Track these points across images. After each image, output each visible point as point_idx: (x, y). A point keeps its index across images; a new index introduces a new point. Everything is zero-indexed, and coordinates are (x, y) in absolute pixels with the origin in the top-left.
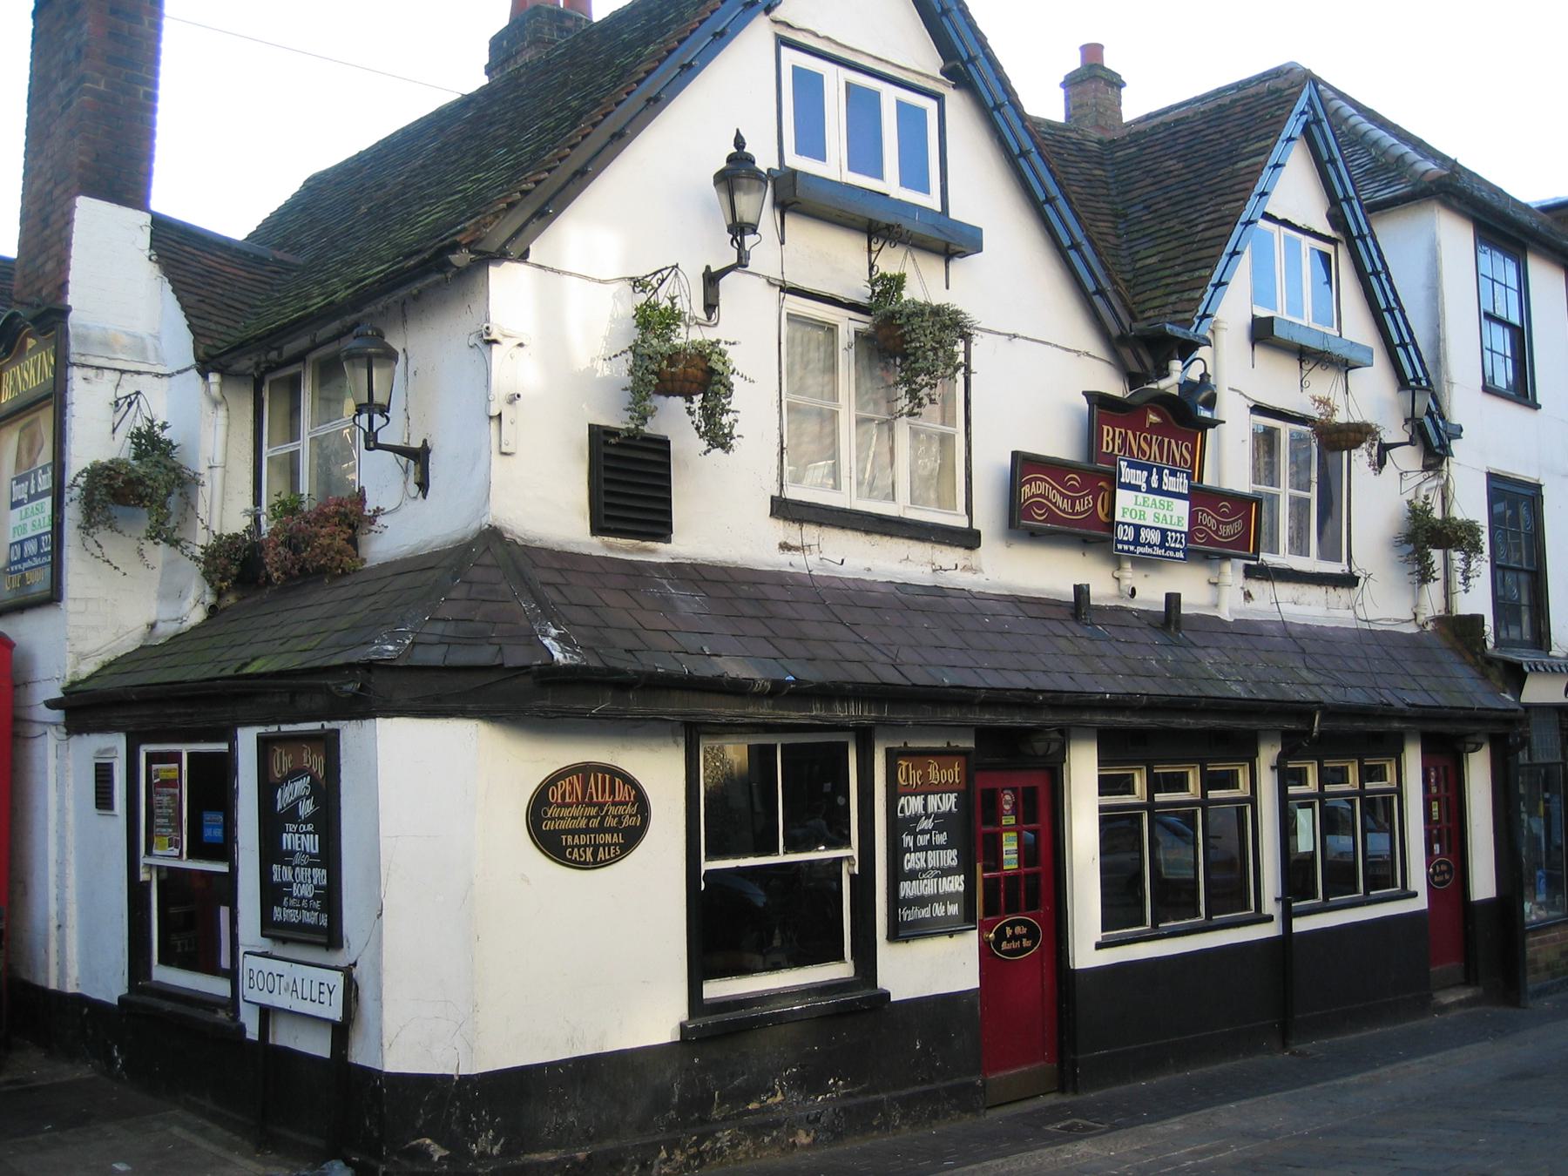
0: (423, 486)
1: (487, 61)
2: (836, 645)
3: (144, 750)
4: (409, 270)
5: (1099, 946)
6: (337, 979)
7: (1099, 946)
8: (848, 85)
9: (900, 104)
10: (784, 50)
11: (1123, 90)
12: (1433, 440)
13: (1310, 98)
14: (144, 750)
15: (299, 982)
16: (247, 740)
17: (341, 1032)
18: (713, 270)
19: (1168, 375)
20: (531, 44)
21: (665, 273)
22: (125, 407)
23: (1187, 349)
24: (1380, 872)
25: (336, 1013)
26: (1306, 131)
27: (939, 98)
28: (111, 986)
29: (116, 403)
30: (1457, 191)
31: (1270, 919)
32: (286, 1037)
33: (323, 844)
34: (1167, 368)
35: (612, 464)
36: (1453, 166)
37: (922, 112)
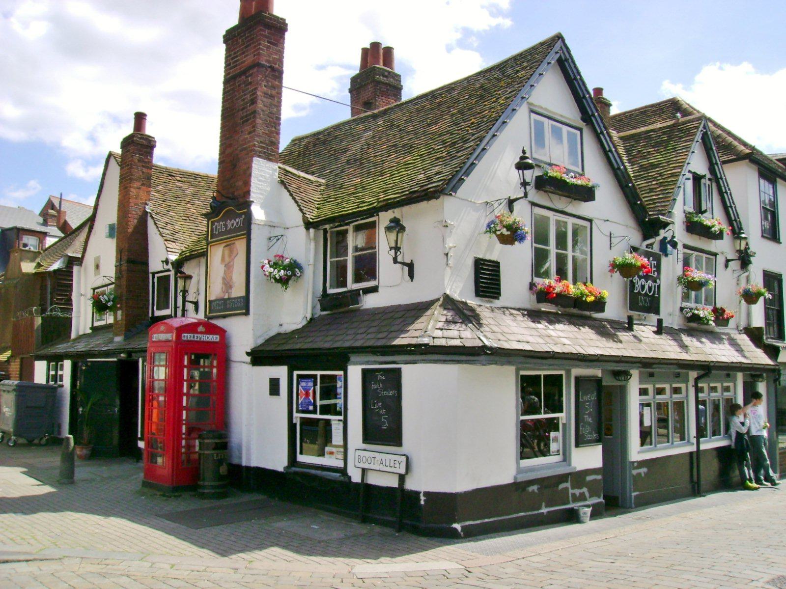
0: (411, 275)
1: (349, 87)
2: (491, 331)
3: (296, 373)
4: (414, 198)
5: (639, 452)
6: (404, 459)
7: (639, 452)
8: (552, 125)
9: (568, 132)
10: (532, 114)
11: (611, 108)
12: (744, 259)
13: (704, 125)
14: (296, 373)
15: (384, 461)
16: (355, 373)
17: (402, 478)
18: (511, 198)
19: (659, 235)
20: (371, 82)
21: (502, 201)
22: (275, 240)
23: (665, 225)
24: (662, 424)
25: (402, 471)
26: (702, 138)
27: (580, 130)
28: (278, 462)
29: (270, 239)
30: (753, 157)
31: (693, 444)
32: (374, 480)
33: (680, 426)
34: (658, 232)
35: (768, 333)
36: (753, 148)
37: (576, 135)
